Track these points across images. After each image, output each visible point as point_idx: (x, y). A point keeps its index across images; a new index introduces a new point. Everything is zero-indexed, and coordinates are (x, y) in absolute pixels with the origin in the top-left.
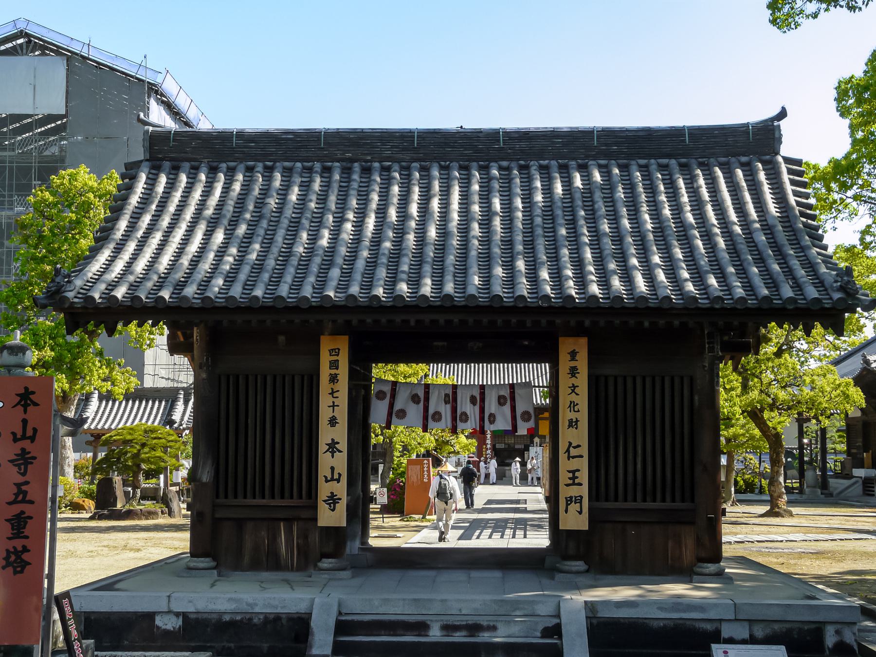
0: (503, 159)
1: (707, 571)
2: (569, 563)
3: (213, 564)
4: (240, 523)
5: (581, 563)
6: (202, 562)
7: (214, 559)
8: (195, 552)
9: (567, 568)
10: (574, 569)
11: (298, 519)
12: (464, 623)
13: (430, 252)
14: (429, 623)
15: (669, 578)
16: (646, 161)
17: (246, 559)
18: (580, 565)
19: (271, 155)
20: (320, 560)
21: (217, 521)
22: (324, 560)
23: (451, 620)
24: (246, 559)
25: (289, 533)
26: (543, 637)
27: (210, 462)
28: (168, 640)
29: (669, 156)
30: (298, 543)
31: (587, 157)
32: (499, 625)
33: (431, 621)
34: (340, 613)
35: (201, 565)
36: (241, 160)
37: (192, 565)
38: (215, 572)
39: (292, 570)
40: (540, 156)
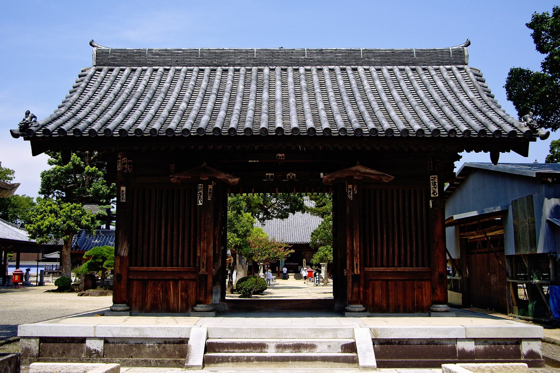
0: (307, 65)
1: (439, 309)
2: (353, 306)
3: (128, 308)
4: (144, 283)
5: (361, 306)
6: (120, 306)
7: (128, 305)
8: (115, 302)
9: (353, 309)
10: (357, 310)
11: (182, 279)
12: (291, 343)
13: (265, 107)
14: (267, 343)
15: (416, 314)
16: (392, 67)
17: (148, 306)
18: (360, 307)
19: (168, 62)
20: (195, 306)
21: (130, 282)
22: (198, 305)
23: (284, 341)
24: (148, 306)
25: (176, 287)
26: (344, 351)
27: (126, 243)
28: (466, 357)
29: (405, 64)
30: (182, 296)
31: (357, 64)
32: (508, 115)
33: (270, 342)
34: (208, 338)
35: (119, 309)
36: (151, 66)
37: (114, 308)
38: (128, 313)
39: (177, 312)
40: (329, 63)
